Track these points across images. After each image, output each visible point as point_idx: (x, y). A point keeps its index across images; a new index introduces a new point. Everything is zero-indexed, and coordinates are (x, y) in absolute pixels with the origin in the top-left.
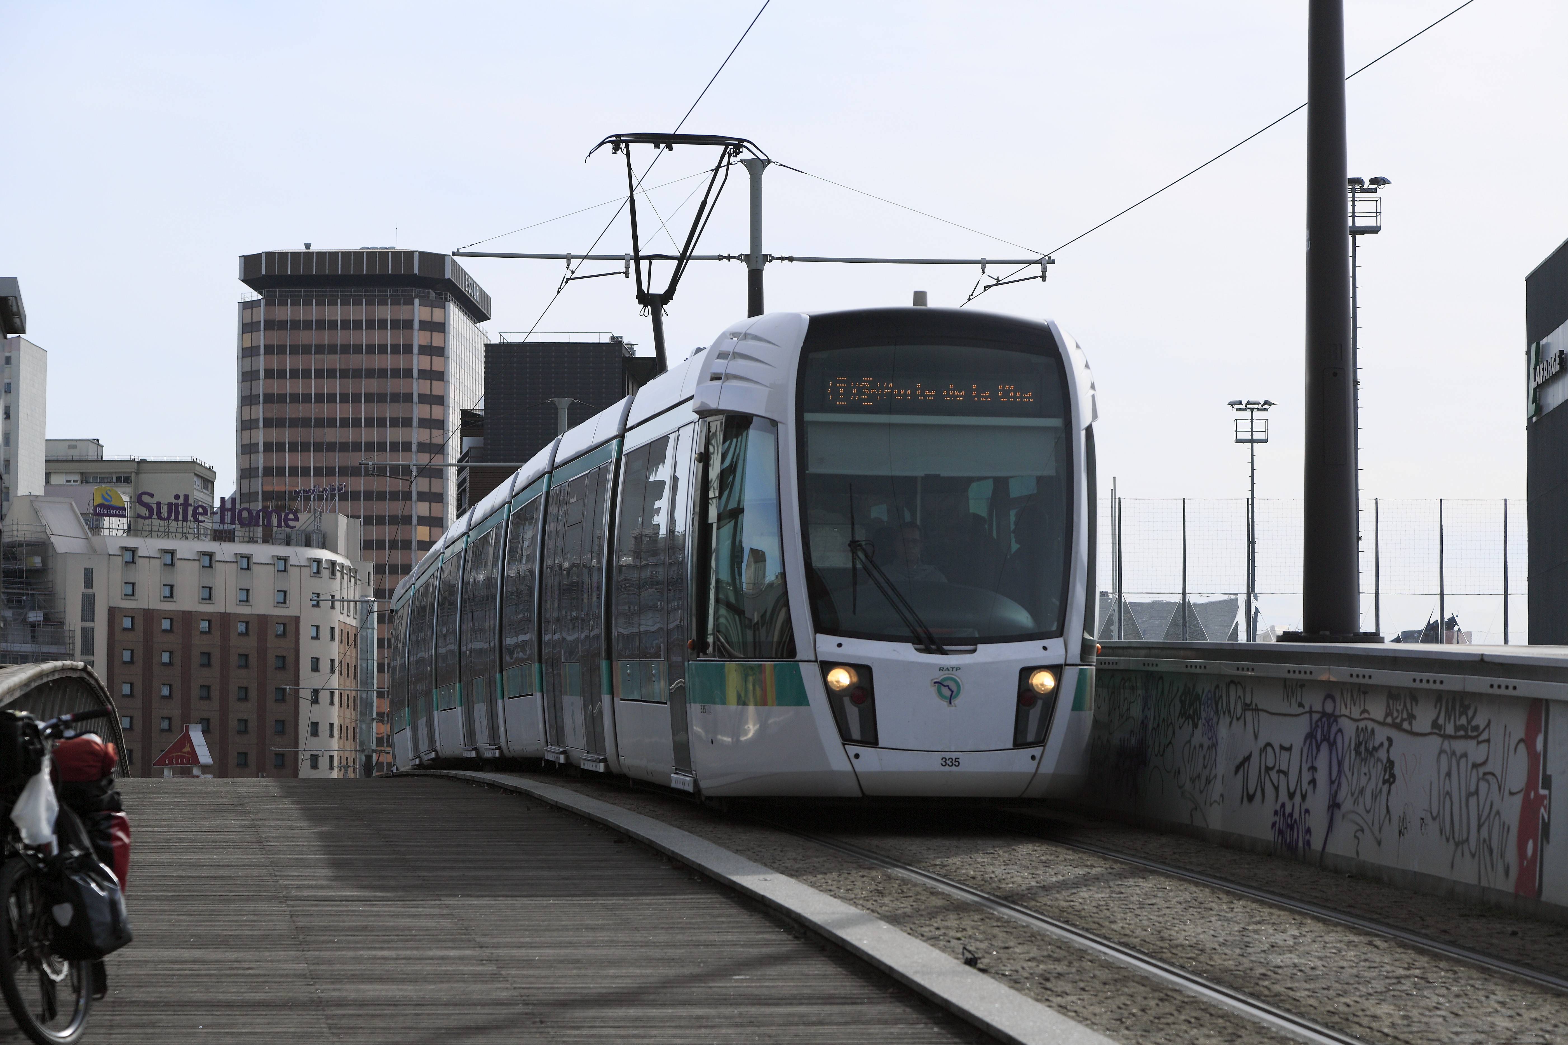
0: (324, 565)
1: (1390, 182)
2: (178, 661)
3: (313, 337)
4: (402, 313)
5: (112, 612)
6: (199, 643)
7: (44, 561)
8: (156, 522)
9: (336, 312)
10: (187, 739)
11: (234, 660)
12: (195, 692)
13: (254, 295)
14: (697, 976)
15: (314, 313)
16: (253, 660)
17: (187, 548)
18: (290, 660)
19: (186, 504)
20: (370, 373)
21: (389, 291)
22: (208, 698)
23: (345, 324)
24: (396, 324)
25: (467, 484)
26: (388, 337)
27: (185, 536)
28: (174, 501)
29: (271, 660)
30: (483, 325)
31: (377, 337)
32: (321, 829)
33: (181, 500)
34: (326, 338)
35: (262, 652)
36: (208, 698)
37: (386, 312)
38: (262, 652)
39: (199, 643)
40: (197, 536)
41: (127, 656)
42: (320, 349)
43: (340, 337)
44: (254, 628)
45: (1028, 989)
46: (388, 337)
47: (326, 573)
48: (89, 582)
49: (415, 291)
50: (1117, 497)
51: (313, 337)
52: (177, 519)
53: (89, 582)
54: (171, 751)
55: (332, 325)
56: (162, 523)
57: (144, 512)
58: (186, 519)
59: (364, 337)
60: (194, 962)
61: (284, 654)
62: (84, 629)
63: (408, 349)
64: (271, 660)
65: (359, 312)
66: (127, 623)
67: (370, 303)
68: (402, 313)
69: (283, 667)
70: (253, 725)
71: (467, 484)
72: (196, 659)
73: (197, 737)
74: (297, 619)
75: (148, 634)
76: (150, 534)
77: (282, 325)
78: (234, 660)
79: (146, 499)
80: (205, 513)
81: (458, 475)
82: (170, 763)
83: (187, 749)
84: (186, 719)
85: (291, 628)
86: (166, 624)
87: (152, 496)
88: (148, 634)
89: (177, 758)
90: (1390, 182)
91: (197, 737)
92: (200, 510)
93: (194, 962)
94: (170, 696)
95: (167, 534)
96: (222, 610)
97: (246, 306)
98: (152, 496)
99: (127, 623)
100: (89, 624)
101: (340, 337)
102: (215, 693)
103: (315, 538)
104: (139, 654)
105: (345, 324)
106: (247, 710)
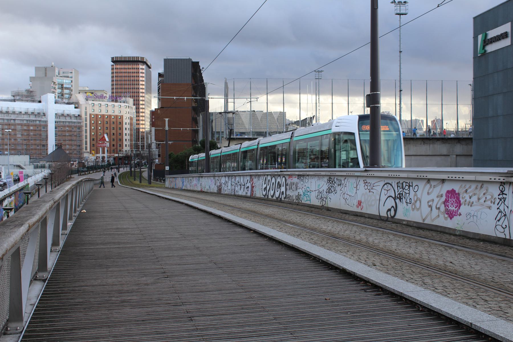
0: (127, 106)
1: (391, 3)
2: (102, 123)
4: (138, 67)
5: (90, 115)
6: (106, 120)
7: (78, 106)
9: (127, 67)
10: (104, 137)
11: (112, 123)
12: (105, 128)
14: (446, 234)
15: (123, 67)
17: (103, 103)
18: (121, 123)
19: (103, 96)
20: (132, 76)
22: (107, 129)
24: (136, 68)
26: (135, 71)
27: (103, 101)
29: (118, 123)
30: (150, 69)
31: (133, 71)
34: (125, 71)
35: (117, 122)
36: (107, 129)
37: (135, 66)
39: (106, 120)
40: (105, 101)
42: (124, 73)
43: (127, 71)
44: (115, 117)
45: (93, 154)
47: (127, 108)
48: (86, 109)
53: (86, 109)
57: (95, 97)
59: (131, 71)
62: (85, 117)
63: (139, 73)
64: (118, 123)
65: (130, 67)
66: (93, 116)
67: (132, 65)
68: (138, 67)
69: (120, 124)
70: (95, 139)
71: (160, 87)
72: (105, 123)
73: (106, 136)
74: (123, 116)
75: (97, 118)
76: (97, 101)
77: (118, 68)
78: (112, 123)
79: (96, 95)
81: (158, 85)
83: (104, 138)
84: (104, 133)
85: (122, 117)
88: (97, 118)
90: (391, 3)
91: (106, 136)
94: (101, 129)
95: (99, 101)
97: (112, 65)
100: (86, 122)
101: (127, 71)
102: (109, 128)
103: (125, 102)
104: (95, 121)
106: (114, 131)
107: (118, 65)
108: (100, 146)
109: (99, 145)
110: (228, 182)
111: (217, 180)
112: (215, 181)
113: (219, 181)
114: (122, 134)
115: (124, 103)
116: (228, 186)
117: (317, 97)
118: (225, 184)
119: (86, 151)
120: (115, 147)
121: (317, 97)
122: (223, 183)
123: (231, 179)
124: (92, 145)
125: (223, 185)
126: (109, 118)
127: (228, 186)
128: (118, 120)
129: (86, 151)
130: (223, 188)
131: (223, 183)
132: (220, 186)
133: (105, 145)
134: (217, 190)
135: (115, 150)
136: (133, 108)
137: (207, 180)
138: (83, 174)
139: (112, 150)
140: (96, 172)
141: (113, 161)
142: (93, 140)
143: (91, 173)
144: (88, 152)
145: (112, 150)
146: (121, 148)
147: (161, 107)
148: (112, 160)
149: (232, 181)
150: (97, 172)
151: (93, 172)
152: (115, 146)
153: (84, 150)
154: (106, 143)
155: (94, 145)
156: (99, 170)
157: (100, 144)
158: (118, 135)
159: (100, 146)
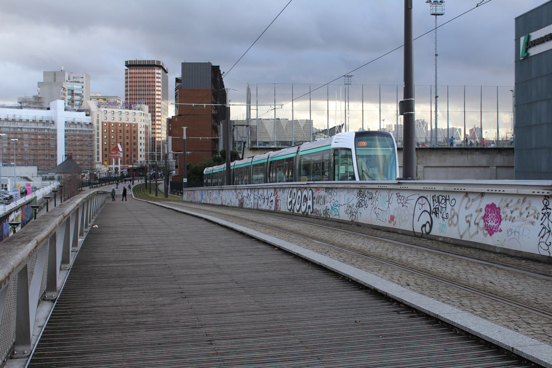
0: (142, 114)
1: (426, 2)
2: (115, 131)
3: (138, 75)
4: (153, 71)
5: (103, 123)
6: (119, 128)
7: (89, 113)
8: (110, 106)
9: (142, 71)
11: (126, 131)
13: (127, 68)
15: (138, 71)
16: (129, 131)
17: (116, 111)
19: (116, 102)
21: (151, 67)
22: (121, 138)
23: (143, 73)
25: (178, 93)
26: (151, 75)
27: (116, 108)
29: (133, 132)
31: (149, 75)
32: (302, 165)
34: (140, 75)
35: (131, 130)
36: (121, 138)
37: (151, 71)
38: (131, 130)
39: (119, 128)
41: (105, 131)
43: (142, 75)
45: (105, 165)
46: (151, 75)
47: (142, 115)
48: (98, 117)
49: (156, 67)
50: (145, 140)
51: (138, 75)
53: (98, 117)
54: (114, 149)
55: (141, 73)
57: (108, 104)
58: (116, 105)
60: (361, 337)
63: (154, 77)
64: (133, 132)
65: (146, 71)
67: (148, 69)
68: (153, 71)
69: (135, 133)
70: (129, 143)
71: (178, 93)
73: (119, 145)
74: (137, 124)
75: (109, 127)
76: (109, 108)
79: (108, 101)
80: (120, 104)
84: (117, 143)
86: (113, 125)
88: (109, 127)
90: (426, 2)
91: (119, 145)
93: (361, 337)
95: (112, 108)
96: (123, 122)
97: (126, 70)
99: (105, 124)
101: (142, 75)
102: (122, 138)
103: (140, 109)
104: (108, 131)
105: (143, 73)
106: (128, 141)
107: (132, 69)
109: (112, 156)
110: (250, 195)
111: (239, 193)
112: (237, 194)
113: (241, 194)
114: (136, 144)
117: (347, 104)
118: (247, 197)
119: (98, 162)
120: (129, 158)
121: (347, 104)
123: (253, 192)
124: (104, 156)
125: (245, 199)
126: (122, 126)
128: (133, 128)
129: (98, 162)
132: (242, 199)
133: (118, 155)
134: (239, 204)
135: (129, 161)
136: (149, 116)
137: (228, 193)
139: (126, 160)
140: (108, 185)
141: (127, 173)
142: (106, 150)
144: (100, 163)
145: (126, 160)
148: (126, 172)
150: (110, 184)
151: (106, 185)
152: (129, 156)
153: (96, 161)
154: (119, 154)
155: (106, 155)
156: (112, 182)
158: (132, 145)
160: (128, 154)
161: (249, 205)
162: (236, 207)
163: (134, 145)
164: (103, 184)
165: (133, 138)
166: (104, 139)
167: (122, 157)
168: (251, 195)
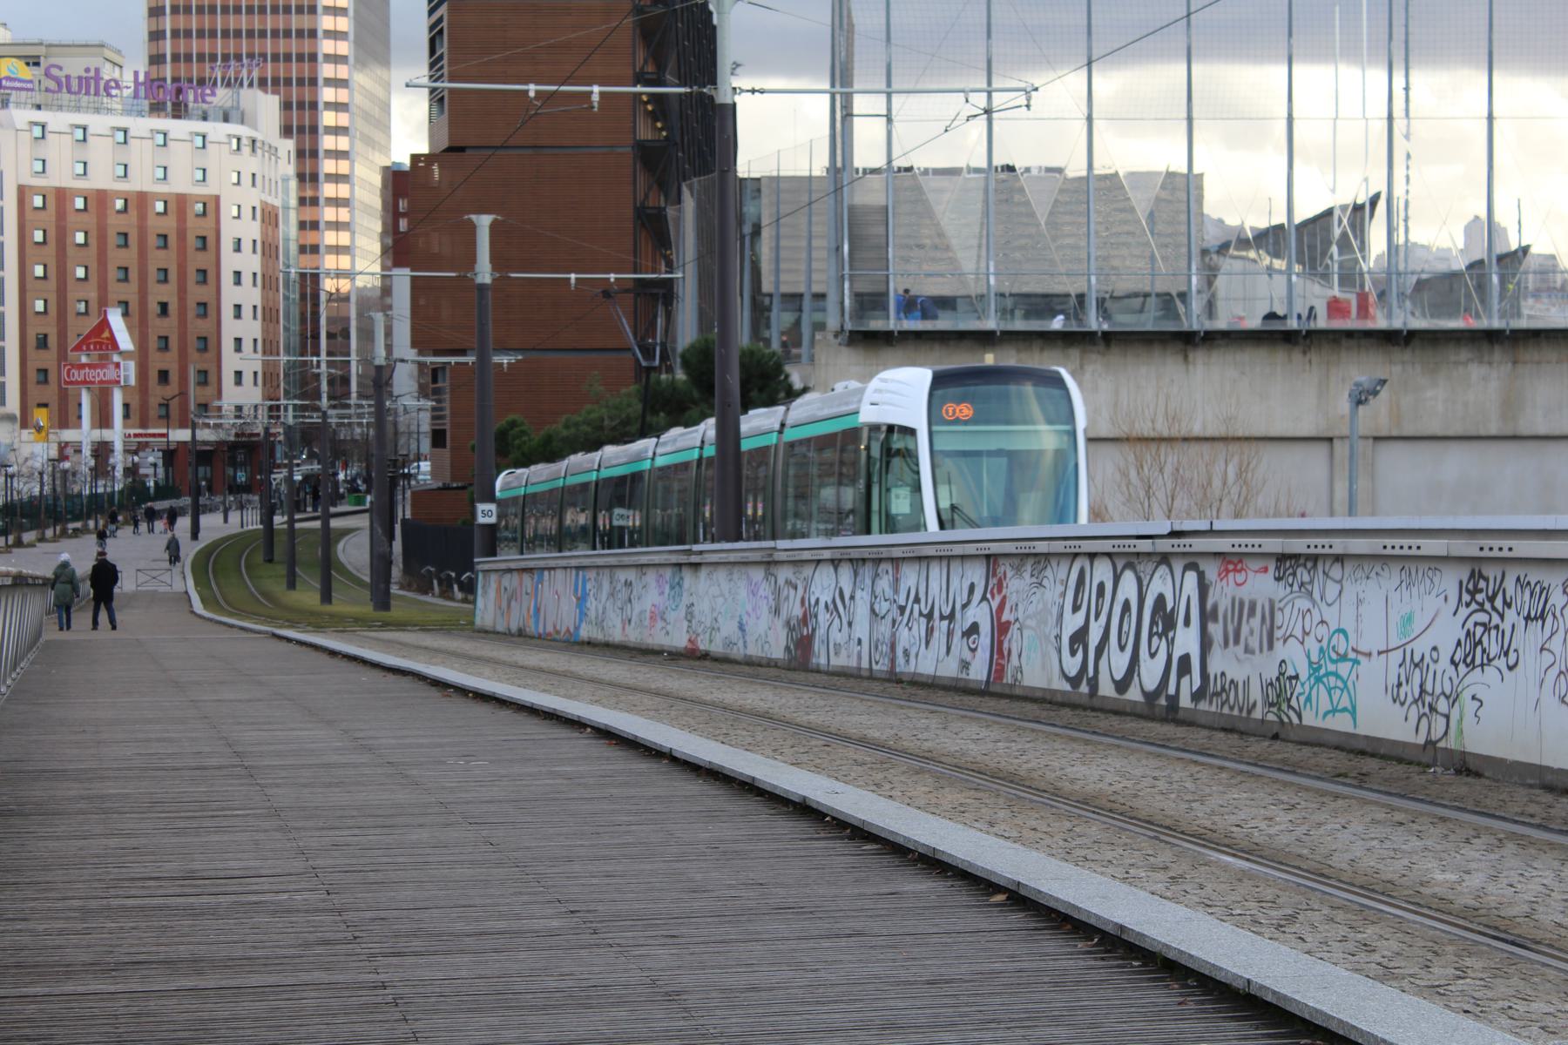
0: (244, 141)
2: (93, 241)
16: (173, 240)
28: (84, 75)
29: (192, 242)
33: (92, 74)
44: (172, 207)
47: (246, 150)
52: (87, 93)
56: (73, 97)
61: (204, 234)
64: (192, 242)
69: (204, 248)
82: (88, 349)
83: (106, 334)
85: (211, 207)
87: (60, 68)
89: (95, 343)
92: (113, 84)
95: (78, 109)
98: (60, 68)
103: (234, 115)
108: (85, 382)
109: (77, 375)
110: (852, 598)
111: (788, 583)
112: (777, 592)
114: (211, 311)
115: (226, 119)
116: (850, 624)
118: (832, 608)
120: (173, 388)
122: (822, 605)
123: (868, 582)
124: (32, 376)
125: (823, 617)
126: (133, 212)
127: (850, 624)
128: (191, 222)
130: (821, 632)
131: (822, 605)
133: (110, 373)
134: (787, 648)
135: (174, 404)
136: (282, 153)
137: (725, 586)
138: (75, 530)
139: (154, 401)
140: (55, 539)
142: (43, 343)
143: (31, 545)
145: (154, 401)
146: (209, 391)
147: (445, 145)
148: (155, 465)
149: (878, 591)
150: (64, 534)
151: (42, 539)
152: (174, 377)
154: (118, 365)
156: (78, 525)
157: (82, 366)
159: (85, 382)
160: (164, 367)
161: (844, 653)
162: (771, 664)
163: (198, 316)
164: (29, 537)
165: (192, 276)
166: (29, 286)
167: (133, 382)
168: (859, 594)
